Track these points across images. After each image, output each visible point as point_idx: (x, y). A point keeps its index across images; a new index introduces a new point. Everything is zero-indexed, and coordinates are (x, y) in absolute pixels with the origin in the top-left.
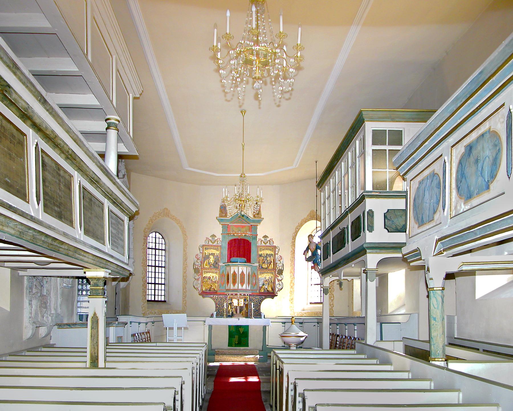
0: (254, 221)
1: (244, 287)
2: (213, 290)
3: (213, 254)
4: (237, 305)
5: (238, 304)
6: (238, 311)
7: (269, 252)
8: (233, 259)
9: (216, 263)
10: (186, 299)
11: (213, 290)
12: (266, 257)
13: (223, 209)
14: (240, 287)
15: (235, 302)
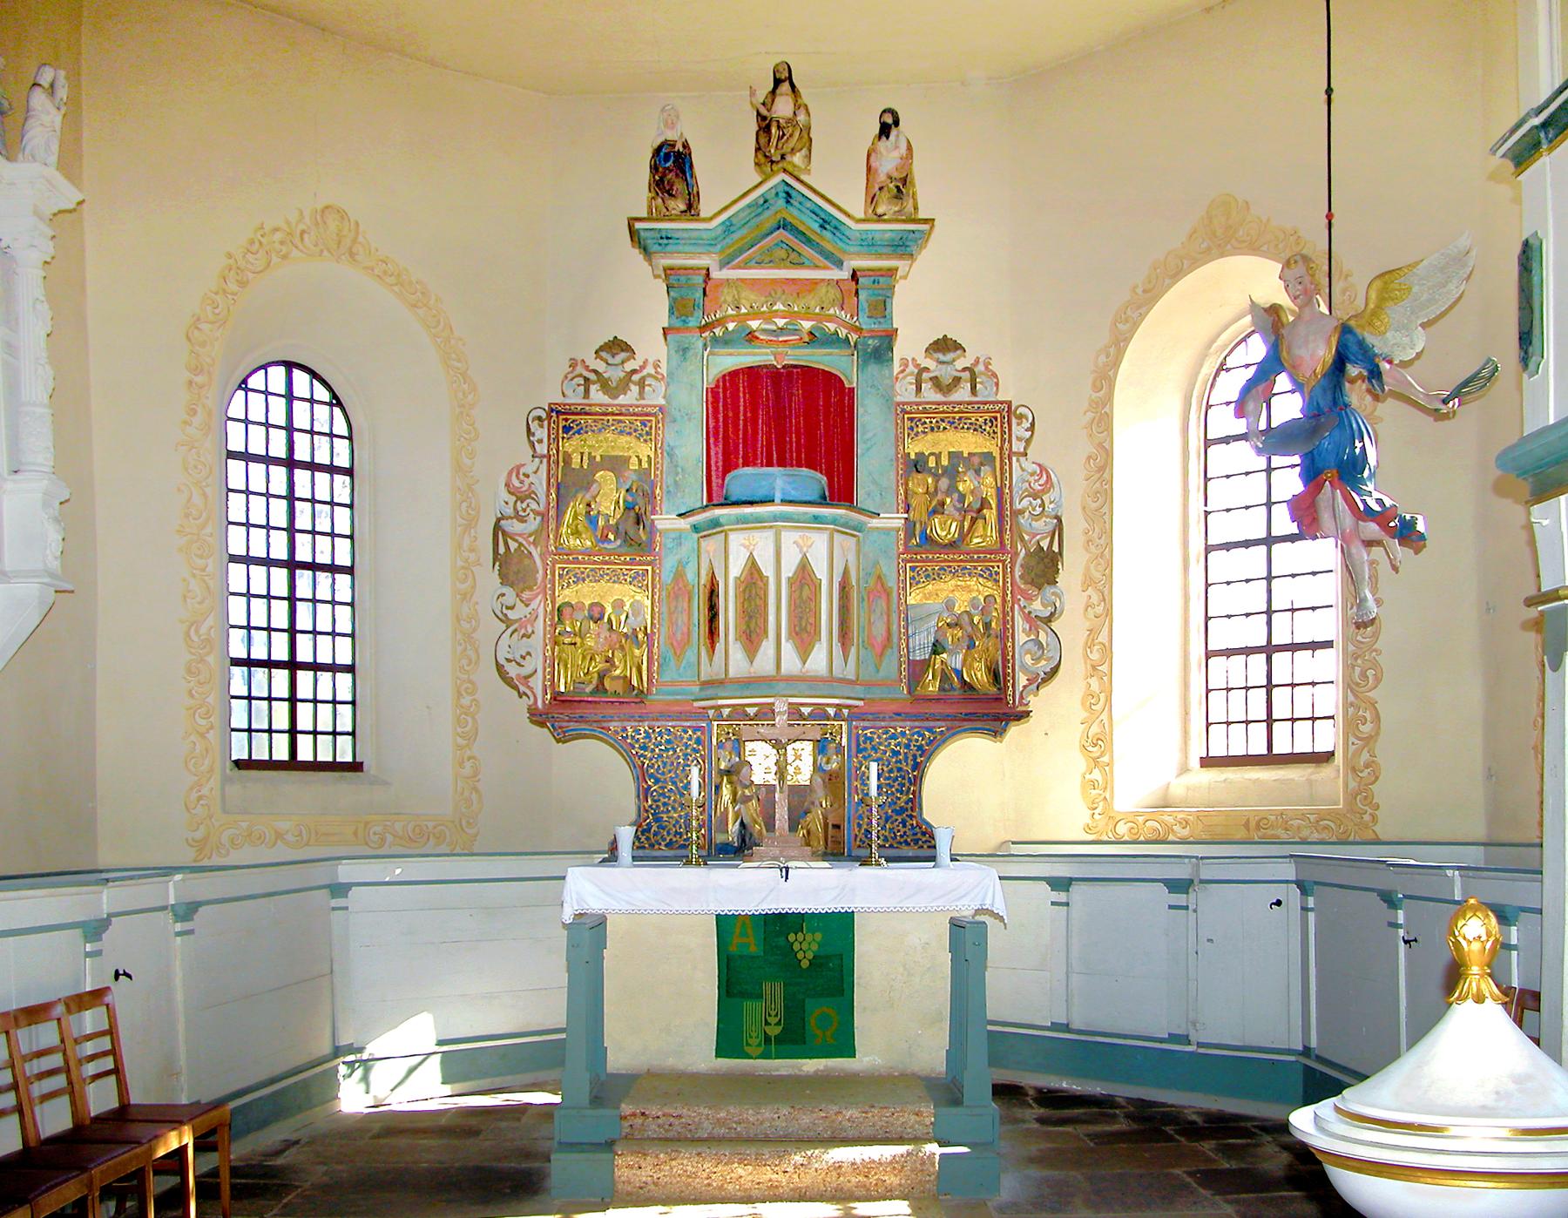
1: (818, 662)
2: (619, 687)
3: (616, 464)
4: (772, 779)
5: (781, 773)
7: (969, 443)
8: (744, 479)
11: (619, 687)
12: (952, 473)
13: (672, 167)
14: (791, 662)
15: (761, 762)
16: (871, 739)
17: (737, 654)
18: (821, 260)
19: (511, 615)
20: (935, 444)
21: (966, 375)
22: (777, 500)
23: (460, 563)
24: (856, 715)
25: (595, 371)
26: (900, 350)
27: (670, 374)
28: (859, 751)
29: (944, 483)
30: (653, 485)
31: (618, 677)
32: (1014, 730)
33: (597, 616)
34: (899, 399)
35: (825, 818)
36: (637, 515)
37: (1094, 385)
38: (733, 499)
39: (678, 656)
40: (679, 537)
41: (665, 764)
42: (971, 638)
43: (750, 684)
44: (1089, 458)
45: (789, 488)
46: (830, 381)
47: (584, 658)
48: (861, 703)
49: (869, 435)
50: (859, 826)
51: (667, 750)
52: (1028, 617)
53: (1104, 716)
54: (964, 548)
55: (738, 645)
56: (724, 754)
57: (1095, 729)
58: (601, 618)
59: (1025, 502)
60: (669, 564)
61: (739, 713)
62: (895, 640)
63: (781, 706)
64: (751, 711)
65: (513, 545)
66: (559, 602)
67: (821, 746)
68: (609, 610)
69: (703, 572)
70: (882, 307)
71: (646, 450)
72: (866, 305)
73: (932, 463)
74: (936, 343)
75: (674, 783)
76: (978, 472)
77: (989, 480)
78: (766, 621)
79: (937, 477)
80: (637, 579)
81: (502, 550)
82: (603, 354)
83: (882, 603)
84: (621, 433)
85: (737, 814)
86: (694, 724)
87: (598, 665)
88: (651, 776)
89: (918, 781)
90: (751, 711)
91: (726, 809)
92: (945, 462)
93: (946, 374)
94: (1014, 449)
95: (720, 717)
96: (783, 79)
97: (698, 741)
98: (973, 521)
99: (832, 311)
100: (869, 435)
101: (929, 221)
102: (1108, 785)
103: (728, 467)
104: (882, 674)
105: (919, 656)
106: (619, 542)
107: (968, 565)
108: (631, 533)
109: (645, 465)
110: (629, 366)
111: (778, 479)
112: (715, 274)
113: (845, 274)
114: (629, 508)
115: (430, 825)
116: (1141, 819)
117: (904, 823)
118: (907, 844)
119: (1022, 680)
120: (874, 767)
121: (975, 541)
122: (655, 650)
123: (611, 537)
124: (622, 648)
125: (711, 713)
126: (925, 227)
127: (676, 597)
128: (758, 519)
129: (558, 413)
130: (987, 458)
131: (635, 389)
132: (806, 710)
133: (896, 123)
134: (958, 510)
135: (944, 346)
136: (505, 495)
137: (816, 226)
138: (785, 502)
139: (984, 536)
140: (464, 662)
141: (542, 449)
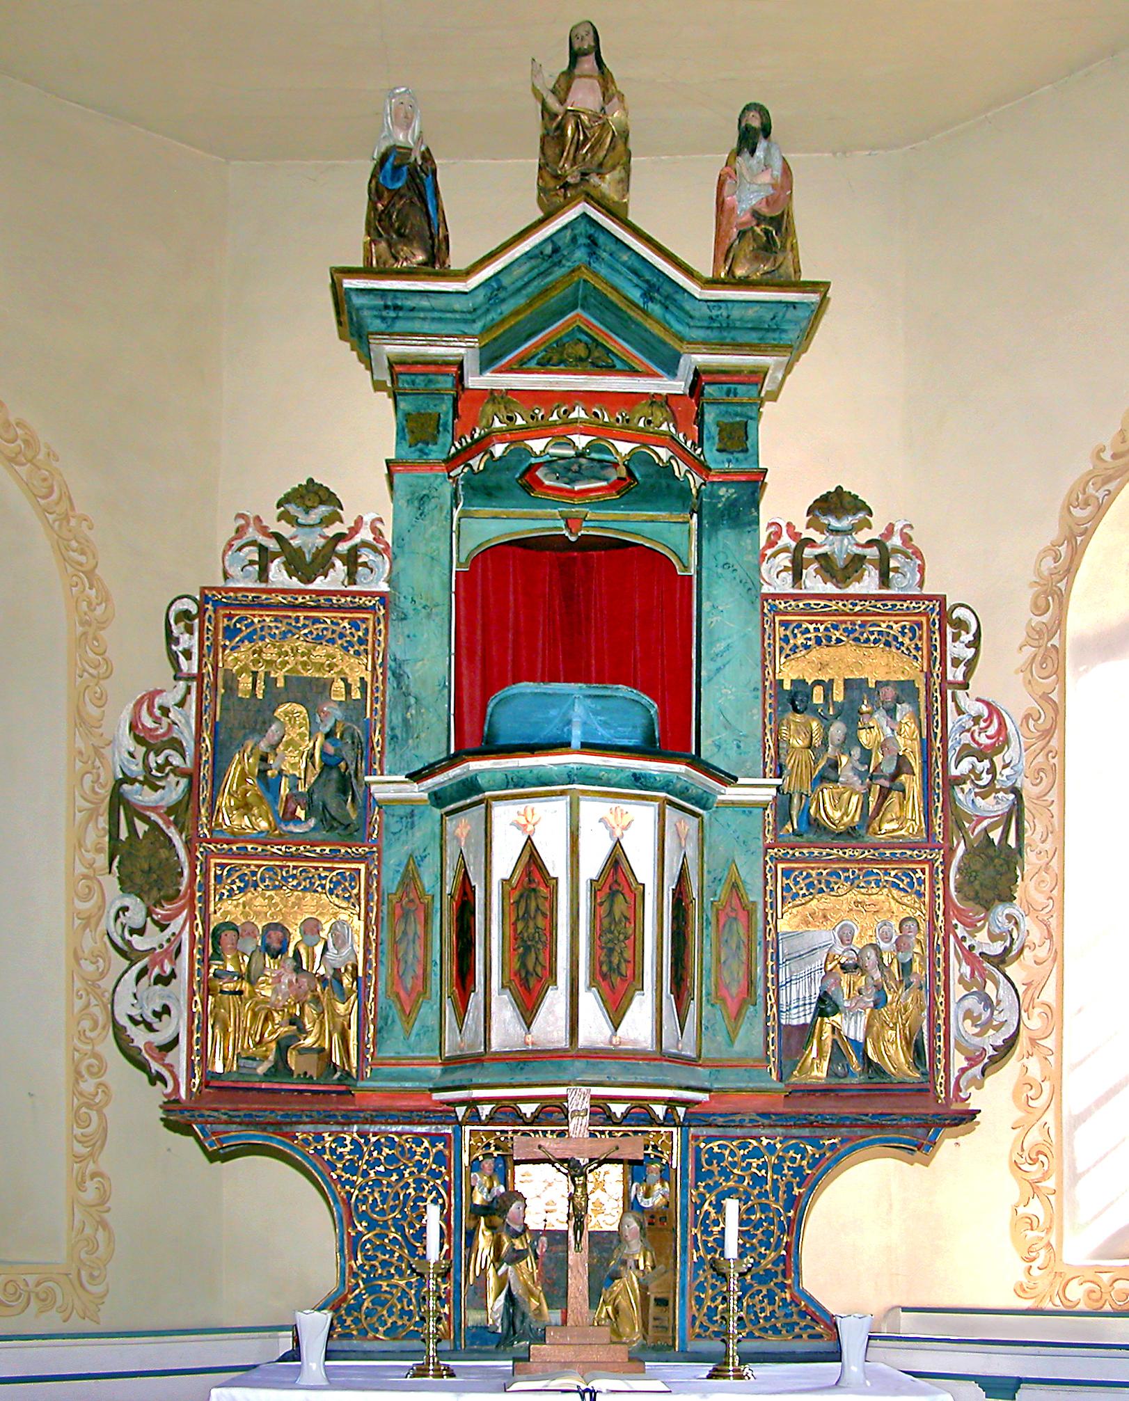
0: (724, 330)
1: (638, 1026)
2: (311, 1065)
3: (310, 692)
4: (558, 1221)
5: (578, 1215)
6: (578, 1283)
7: (879, 666)
8: (522, 702)
9: (341, 776)
10: (105, 1162)
11: (311, 1065)
12: (850, 714)
13: (405, 202)
14: (594, 1028)
15: (542, 1195)
16: (720, 1157)
17: (504, 1012)
18: (640, 359)
19: (139, 942)
20: (823, 666)
21: (873, 552)
22: (576, 743)
23: (80, 869)
24: (697, 1117)
25: (277, 537)
26: (771, 509)
27: (398, 538)
28: (699, 1176)
29: (838, 730)
30: (369, 729)
31: (309, 1049)
32: (950, 1148)
33: (276, 945)
34: (766, 589)
35: (644, 1288)
36: (341, 776)
37: (1035, 605)
38: (502, 741)
39: (408, 1016)
40: (410, 813)
41: (385, 1196)
42: (879, 989)
43: (526, 1060)
44: (1027, 717)
45: (594, 721)
46: (655, 564)
47: (255, 1015)
48: (704, 1097)
49: (721, 646)
50: (699, 1301)
51: (388, 1173)
52: (968, 954)
53: (1049, 1117)
54: (869, 839)
55: (506, 997)
56: (479, 1179)
57: (1034, 1136)
58: (282, 951)
59: (965, 765)
60: (394, 858)
61: (507, 1111)
62: (760, 991)
63: (578, 1100)
64: (528, 1109)
65: (142, 828)
66: (215, 920)
67: (635, 1169)
68: (296, 937)
69: (449, 874)
70: (738, 437)
71: (358, 670)
72: (714, 430)
73: (818, 697)
74: (825, 499)
75: (400, 1229)
76: (891, 712)
77: (909, 728)
78: (553, 956)
79: (826, 721)
80: (340, 885)
81: (124, 834)
82: (292, 508)
83: (740, 928)
84: (319, 639)
85: (502, 1281)
86: (433, 1129)
87: (279, 1028)
88: (363, 1216)
89: (795, 1227)
90: (528, 1109)
91: (484, 1271)
92: (838, 696)
93: (841, 548)
94: (950, 677)
95: (475, 1118)
96: (585, 50)
97: (440, 1158)
98: (884, 794)
99: (664, 427)
100: (721, 646)
101: (820, 287)
102: (1054, 1222)
103: (490, 686)
104: (738, 1047)
105: (799, 1017)
106: (312, 822)
107: (875, 868)
108: (333, 806)
109: (356, 695)
110: (336, 528)
111: (579, 706)
112: (474, 381)
113: (678, 386)
114: (327, 766)
115: (31, 1279)
116: (1106, 1278)
117: (770, 1297)
118: (776, 1331)
119: (959, 1061)
120: (732, 1207)
121: (886, 826)
122: (370, 1005)
123: (301, 813)
124: (317, 1000)
125: (461, 1111)
126: (815, 298)
127: (405, 915)
128: (543, 780)
129: (216, 604)
130: (906, 690)
131: (340, 567)
132: (618, 1109)
133: (766, 131)
134: (861, 775)
135: (835, 503)
136: (128, 743)
137: (636, 295)
138: (588, 747)
139: (901, 819)
140: (87, 1024)
141: (190, 666)
